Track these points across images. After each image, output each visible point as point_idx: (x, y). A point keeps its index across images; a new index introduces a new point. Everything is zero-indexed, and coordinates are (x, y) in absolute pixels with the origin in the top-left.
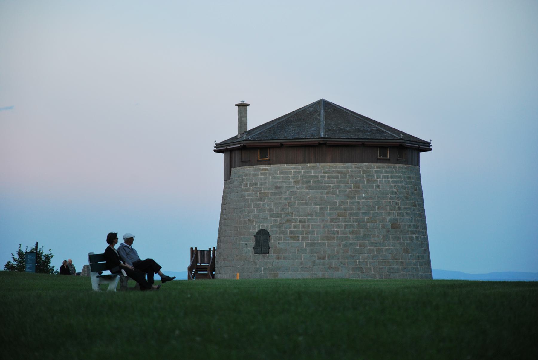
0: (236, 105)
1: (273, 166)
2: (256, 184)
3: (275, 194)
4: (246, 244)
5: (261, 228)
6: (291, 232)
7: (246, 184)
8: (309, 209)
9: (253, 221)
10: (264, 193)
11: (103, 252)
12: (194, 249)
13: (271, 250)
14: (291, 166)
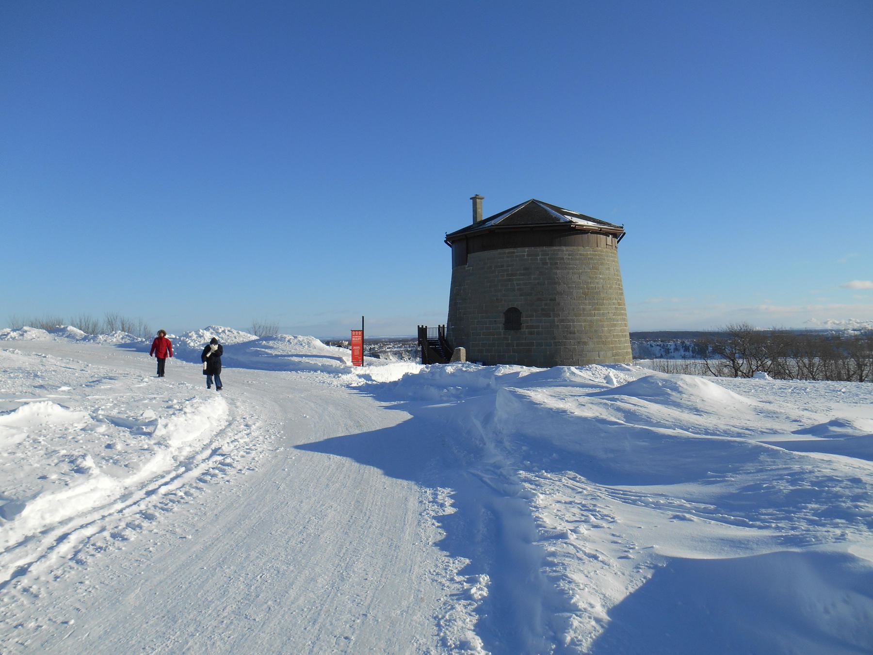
14: (538, 249)
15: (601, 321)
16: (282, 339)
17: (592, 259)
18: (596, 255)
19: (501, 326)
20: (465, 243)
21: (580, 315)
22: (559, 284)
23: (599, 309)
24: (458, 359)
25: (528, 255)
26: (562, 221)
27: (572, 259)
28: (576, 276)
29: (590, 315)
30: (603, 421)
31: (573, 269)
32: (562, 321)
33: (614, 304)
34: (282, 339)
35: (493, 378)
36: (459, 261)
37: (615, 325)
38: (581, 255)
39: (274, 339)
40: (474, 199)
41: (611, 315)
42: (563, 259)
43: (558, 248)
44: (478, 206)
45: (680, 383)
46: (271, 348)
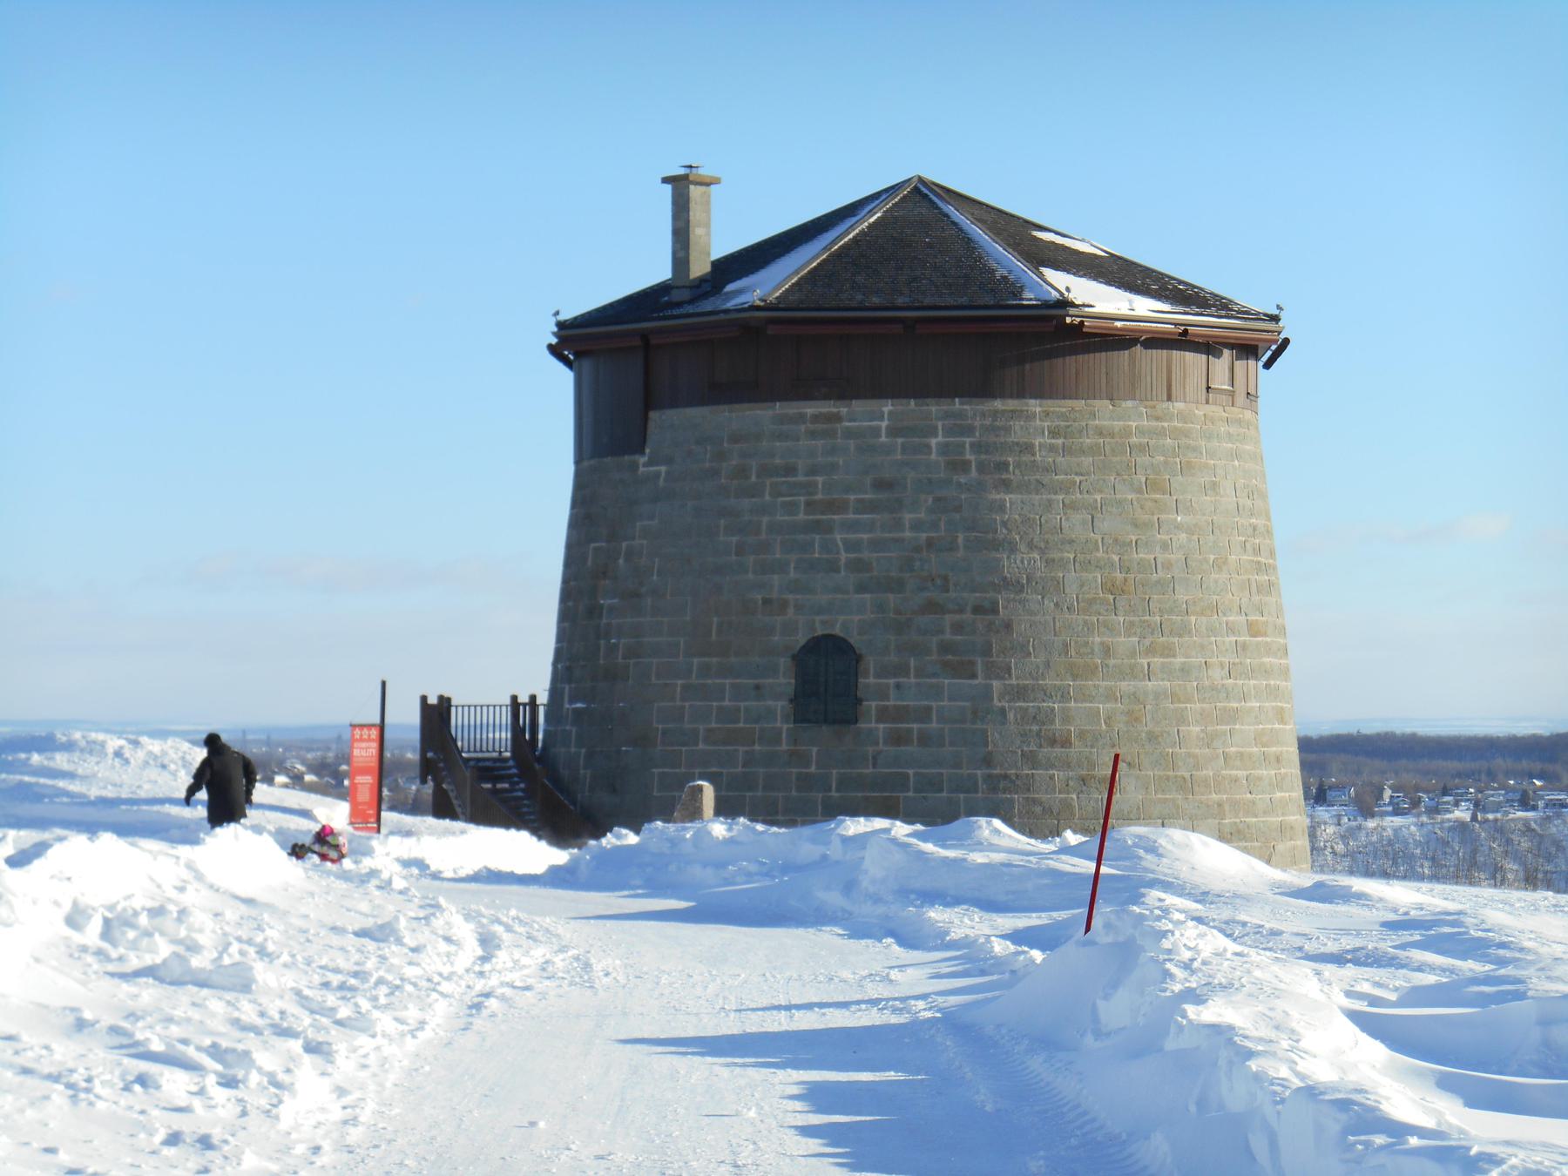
0: (666, 180)
2: (790, 470)
4: (757, 687)
5: (819, 633)
6: (945, 648)
7: (742, 472)
9: (784, 605)
11: (669, 276)
12: (433, 700)
14: (934, 408)
15: (1174, 698)
16: (96, 749)
17: (1143, 449)
18: (1162, 433)
19: (781, 706)
20: (647, 363)
21: (1091, 671)
22: (1013, 549)
23: (1168, 651)
24: (695, 813)
25: (893, 432)
26: (1029, 298)
27: (1066, 450)
28: (1077, 517)
29: (1132, 673)
30: (1009, 865)
31: (1066, 488)
32: (1021, 693)
33: (1231, 629)
34: (96, 749)
35: (836, 843)
36: (607, 434)
37: (1232, 716)
38: (1100, 432)
39: (69, 747)
40: (680, 185)
41: (1217, 674)
42: (1028, 448)
43: (1012, 404)
44: (695, 214)
45: (1162, 841)
46: (71, 776)
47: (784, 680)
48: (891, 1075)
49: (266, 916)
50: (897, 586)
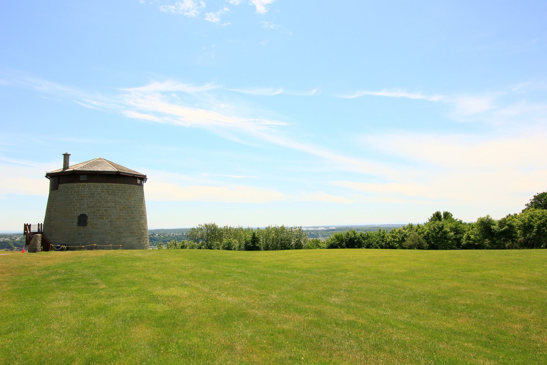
1: (89, 184)
3: (90, 197)
6: (100, 215)
8: (109, 204)
10: (84, 197)
13: (88, 225)
14: (100, 184)
20: (60, 180)
36: (54, 188)
47: (76, 220)
48: (383, 93)
49: (293, 243)
50: (93, 207)
